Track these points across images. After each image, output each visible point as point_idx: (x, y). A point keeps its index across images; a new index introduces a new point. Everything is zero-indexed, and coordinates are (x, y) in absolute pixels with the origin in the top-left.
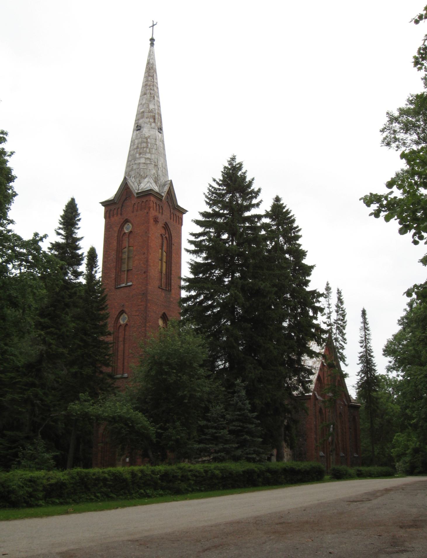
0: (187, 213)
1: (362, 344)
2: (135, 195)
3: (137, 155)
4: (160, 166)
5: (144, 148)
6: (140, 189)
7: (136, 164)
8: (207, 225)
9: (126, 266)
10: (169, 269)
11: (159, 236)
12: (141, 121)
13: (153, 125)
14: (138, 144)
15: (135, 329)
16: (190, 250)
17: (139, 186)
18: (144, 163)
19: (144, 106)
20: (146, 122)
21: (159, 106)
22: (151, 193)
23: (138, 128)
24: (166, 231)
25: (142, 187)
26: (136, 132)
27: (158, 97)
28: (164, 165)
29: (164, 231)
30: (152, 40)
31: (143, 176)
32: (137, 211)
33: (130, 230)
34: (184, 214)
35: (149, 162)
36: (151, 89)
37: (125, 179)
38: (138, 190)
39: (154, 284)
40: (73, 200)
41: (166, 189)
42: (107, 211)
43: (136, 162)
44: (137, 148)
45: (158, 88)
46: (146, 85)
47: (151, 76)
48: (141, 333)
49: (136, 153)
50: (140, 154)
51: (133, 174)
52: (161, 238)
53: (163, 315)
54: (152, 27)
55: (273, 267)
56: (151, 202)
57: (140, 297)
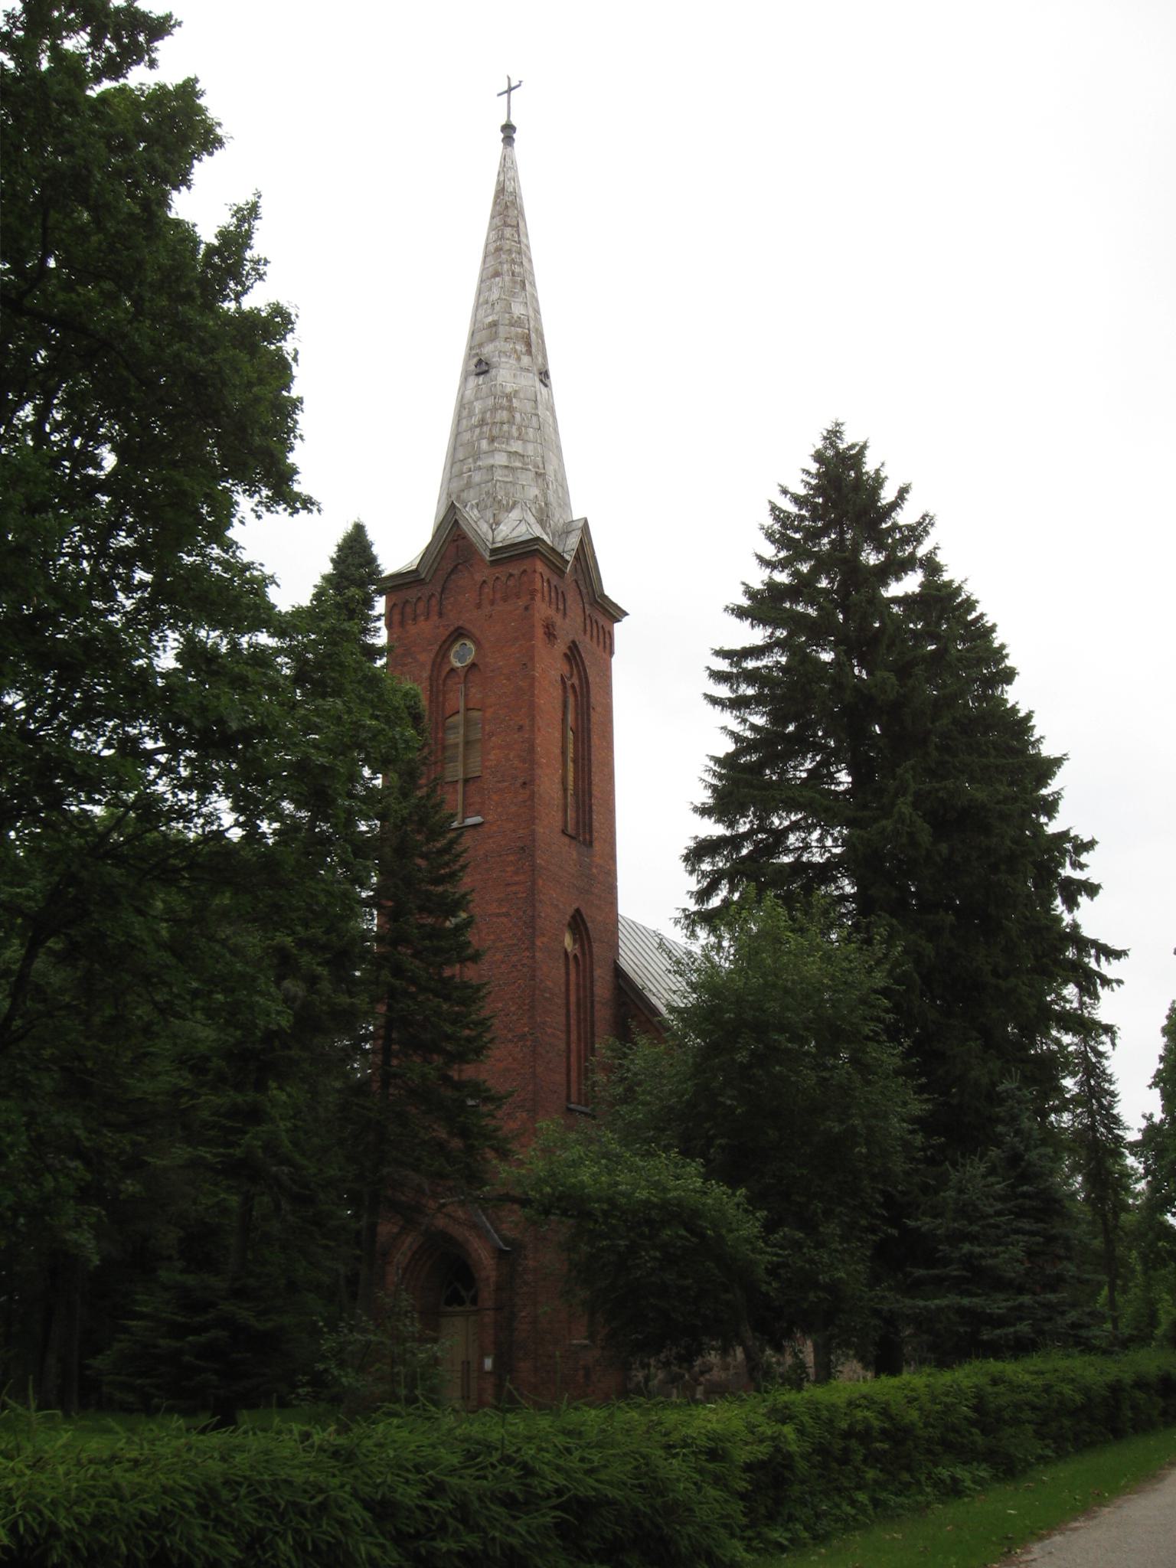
0: (625, 619)
2: (487, 557)
3: (484, 444)
4: (551, 477)
5: (502, 423)
6: (499, 539)
7: (480, 468)
8: (782, 619)
9: (461, 769)
10: (583, 782)
12: (488, 349)
13: (526, 360)
14: (484, 413)
15: (499, 956)
16: (721, 699)
17: (493, 531)
18: (507, 467)
19: (497, 308)
20: (504, 352)
21: (537, 311)
22: (537, 550)
23: (480, 366)
24: (572, 668)
25: (503, 535)
26: (472, 382)
27: (533, 284)
28: (560, 479)
29: (568, 668)
30: (508, 130)
31: (505, 502)
32: (492, 603)
33: (469, 661)
34: (619, 621)
35: (520, 465)
36: (513, 262)
37: (452, 509)
38: (493, 543)
39: (550, 823)
40: (359, 530)
41: (573, 542)
42: (395, 605)
43: (479, 463)
44: (482, 423)
45: (530, 261)
46: (498, 250)
48: (520, 968)
49: (480, 438)
50: (492, 440)
51: (471, 496)
52: (561, 687)
53: (573, 917)
55: (984, 748)
56: (538, 575)
57: (511, 858)
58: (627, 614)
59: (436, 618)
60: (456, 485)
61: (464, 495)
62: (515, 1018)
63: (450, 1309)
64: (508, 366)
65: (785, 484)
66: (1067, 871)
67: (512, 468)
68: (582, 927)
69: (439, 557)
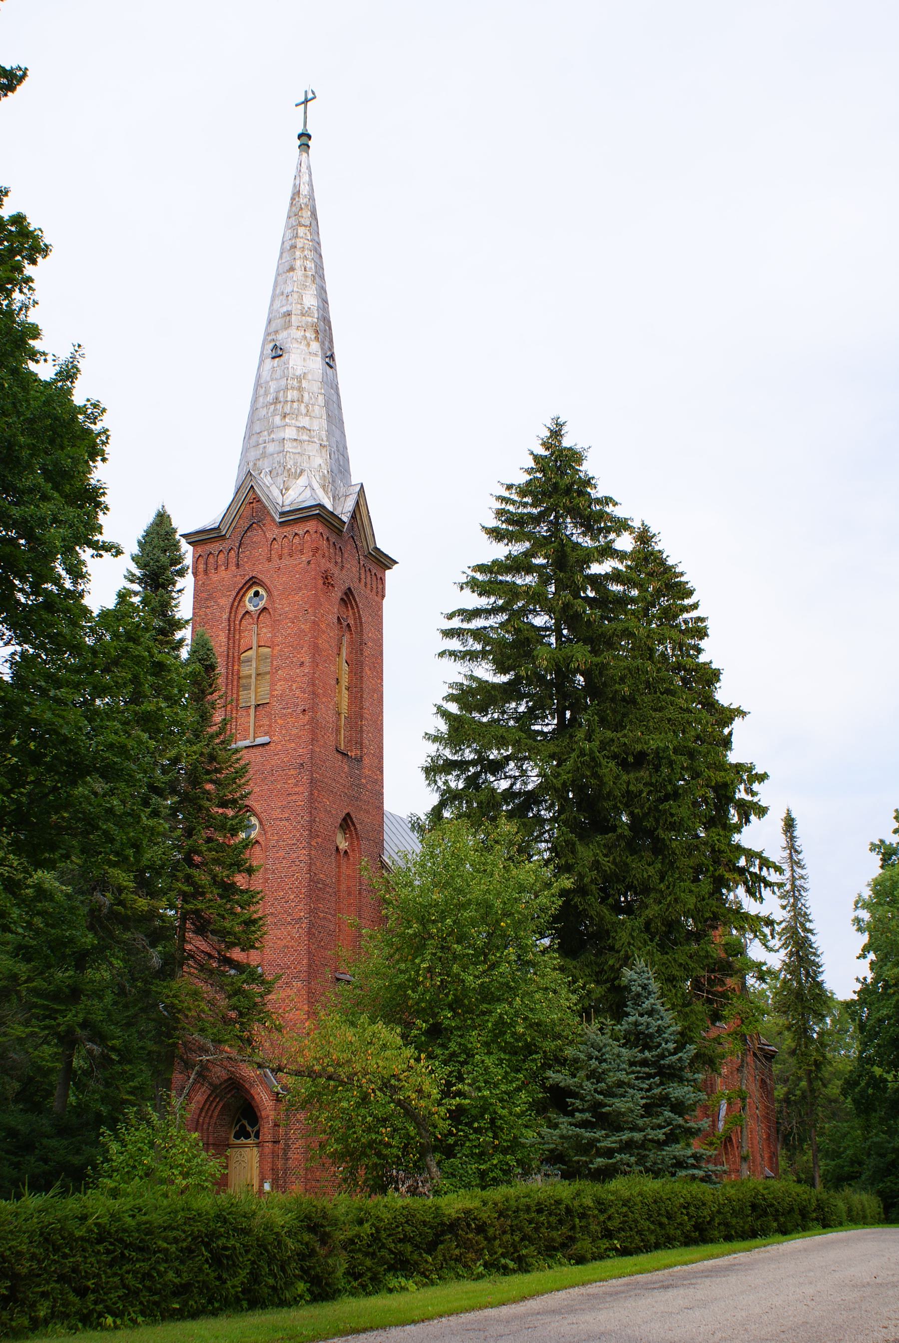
1: (784, 902)
3: (277, 420)
5: (293, 402)
11: (336, 621)
12: (282, 336)
14: (278, 392)
15: (281, 853)
26: (269, 363)
28: (341, 449)
30: (305, 137)
31: (293, 470)
33: (261, 606)
34: (390, 568)
41: (350, 505)
43: (272, 436)
44: (276, 401)
46: (293, 247)
47: (306, 226)
50: (284, 416)
51: (265, 465)
53: (344, 819)
54: (303, 106)
57: (292, 772)
58: (397, 563)
59: (234, 568)
60: (253, 454)
61: (260, 463)
62: (293, 904)
63: (238, 1142)
64: (299, 351)
65: (532, 449)
66: (741, 794)
67: (300, 441)
68: (352, 828)
69: (238, 517)
